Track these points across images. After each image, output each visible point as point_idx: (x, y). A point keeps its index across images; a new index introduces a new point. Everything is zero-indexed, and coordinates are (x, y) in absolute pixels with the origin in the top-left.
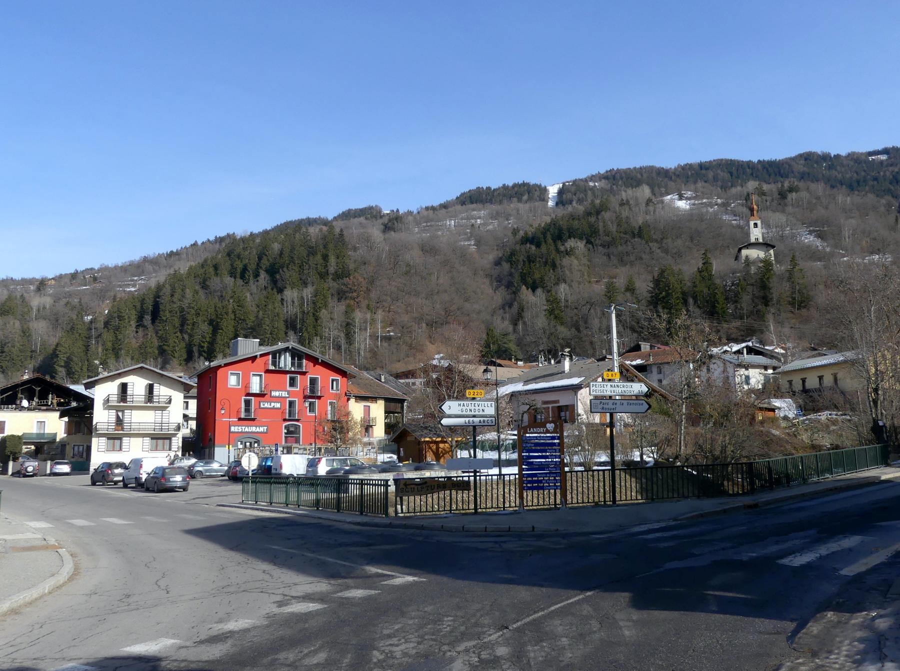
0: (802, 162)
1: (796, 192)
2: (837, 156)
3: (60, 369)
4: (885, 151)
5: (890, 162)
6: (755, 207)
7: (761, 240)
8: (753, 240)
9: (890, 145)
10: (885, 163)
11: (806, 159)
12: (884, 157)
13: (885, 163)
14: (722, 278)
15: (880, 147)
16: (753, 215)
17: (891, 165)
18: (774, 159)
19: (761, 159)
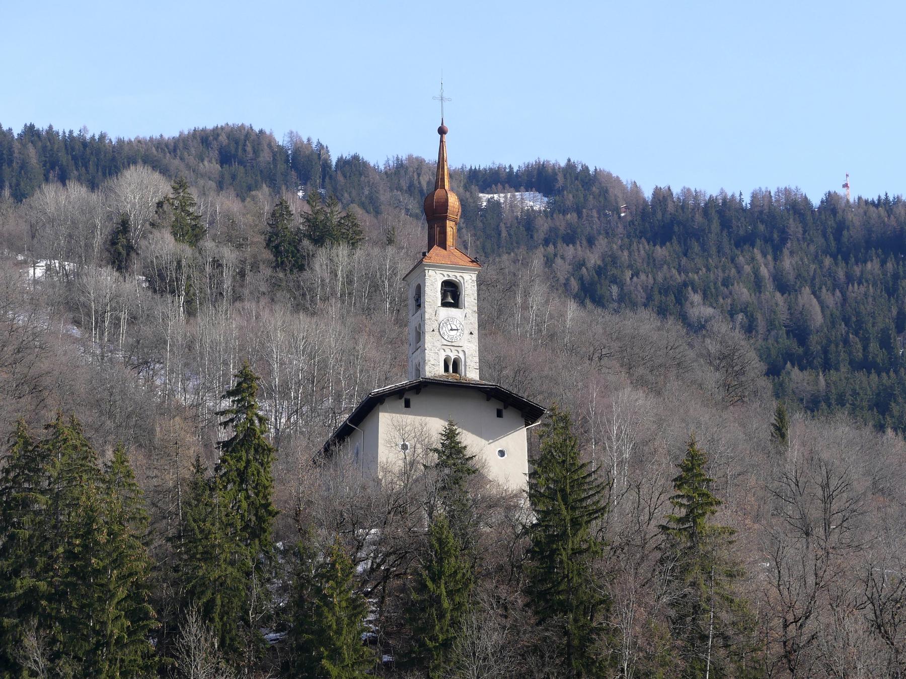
0: (211, 166)
1: (353, 244)
2: (353, 166)
3: (223, 405)
4: (539, 178)
5: (561, 222)
6: (453, 201)
7: (472, 373)
8: (434, 368)
9: (557, 157)
10: (543, 226)
11: (225, 158)
12: (534, 202)
13: (543, 226)
14: (386, 471)
15: (516, 160)
16: (437, 239)
17: (570, 239)
18: (93, 131)
19: (41, 125)
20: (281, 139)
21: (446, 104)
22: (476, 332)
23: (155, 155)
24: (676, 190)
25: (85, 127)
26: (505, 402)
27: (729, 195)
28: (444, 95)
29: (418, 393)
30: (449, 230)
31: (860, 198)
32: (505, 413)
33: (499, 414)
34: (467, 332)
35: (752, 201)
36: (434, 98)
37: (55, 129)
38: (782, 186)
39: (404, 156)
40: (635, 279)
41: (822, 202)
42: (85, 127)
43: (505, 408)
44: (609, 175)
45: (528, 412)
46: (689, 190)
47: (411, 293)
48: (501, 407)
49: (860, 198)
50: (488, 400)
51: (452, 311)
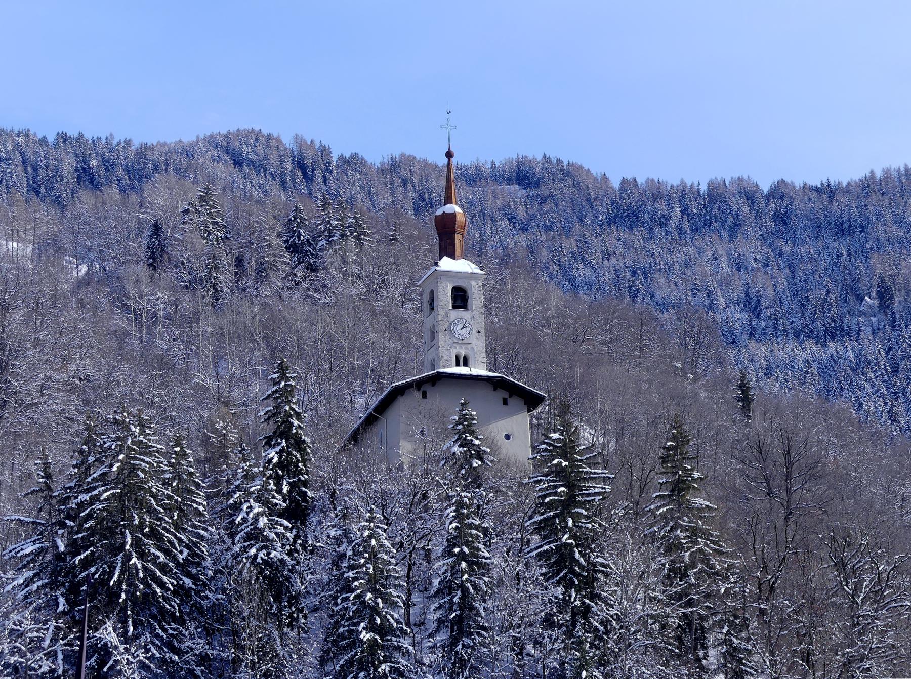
20: (288, 141)
21: (445, 124)
22: (483, 331)
23: (181, 161)
24: (641, 181)
25: (111, 135)
26: (512, 393)
27: (689, 184)
28: (451, 124)
29: (433, 385)
30: (457, 242)
31: (805, 184)
32: (510, 401)
33: (505, 402)
34: (474, 331)
35: (709, 191)
36: (442, 126)
37: (86, 136)
38: (736, 176)
39: (396, 155)
40: (606, 262)
41: (771, 188)
42: (111, 135)
43: (510, 396)
44: (581, 167)
45: (532, 401)
46: (653, 180)
47: (426, 298)
48: (506, 396)
49: (805, 184)
50: (495, 390)
51: (462, 313)
